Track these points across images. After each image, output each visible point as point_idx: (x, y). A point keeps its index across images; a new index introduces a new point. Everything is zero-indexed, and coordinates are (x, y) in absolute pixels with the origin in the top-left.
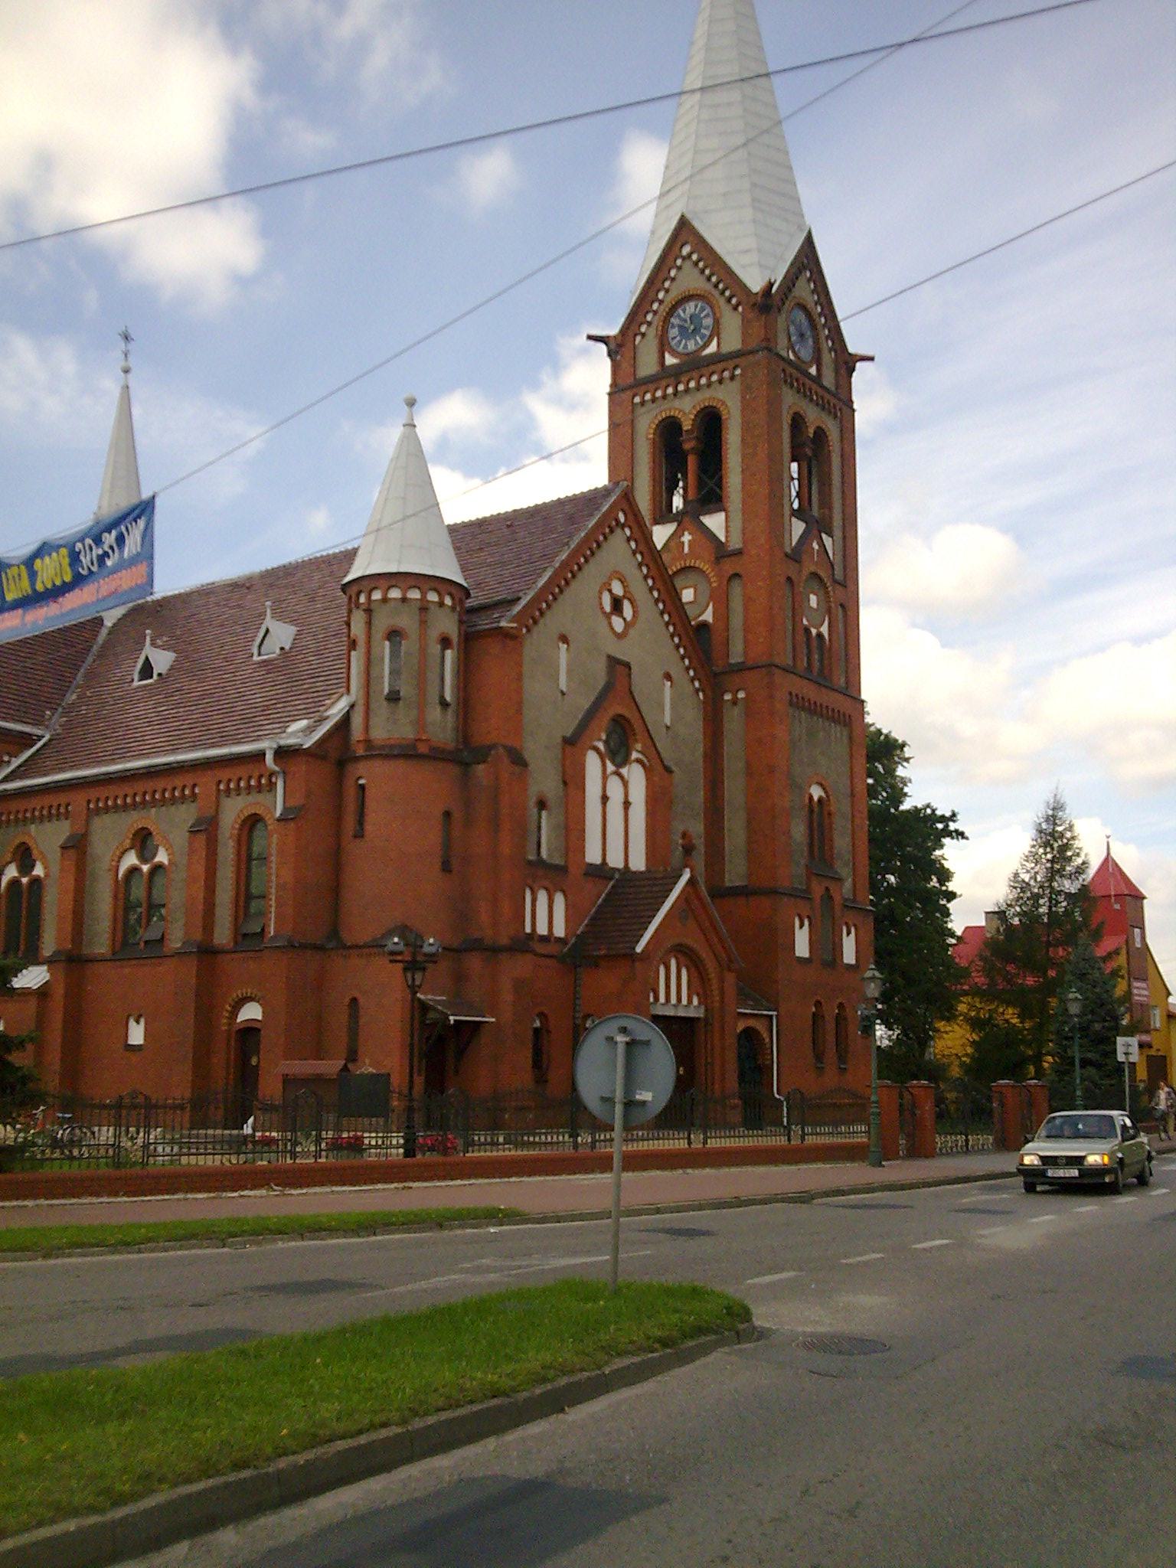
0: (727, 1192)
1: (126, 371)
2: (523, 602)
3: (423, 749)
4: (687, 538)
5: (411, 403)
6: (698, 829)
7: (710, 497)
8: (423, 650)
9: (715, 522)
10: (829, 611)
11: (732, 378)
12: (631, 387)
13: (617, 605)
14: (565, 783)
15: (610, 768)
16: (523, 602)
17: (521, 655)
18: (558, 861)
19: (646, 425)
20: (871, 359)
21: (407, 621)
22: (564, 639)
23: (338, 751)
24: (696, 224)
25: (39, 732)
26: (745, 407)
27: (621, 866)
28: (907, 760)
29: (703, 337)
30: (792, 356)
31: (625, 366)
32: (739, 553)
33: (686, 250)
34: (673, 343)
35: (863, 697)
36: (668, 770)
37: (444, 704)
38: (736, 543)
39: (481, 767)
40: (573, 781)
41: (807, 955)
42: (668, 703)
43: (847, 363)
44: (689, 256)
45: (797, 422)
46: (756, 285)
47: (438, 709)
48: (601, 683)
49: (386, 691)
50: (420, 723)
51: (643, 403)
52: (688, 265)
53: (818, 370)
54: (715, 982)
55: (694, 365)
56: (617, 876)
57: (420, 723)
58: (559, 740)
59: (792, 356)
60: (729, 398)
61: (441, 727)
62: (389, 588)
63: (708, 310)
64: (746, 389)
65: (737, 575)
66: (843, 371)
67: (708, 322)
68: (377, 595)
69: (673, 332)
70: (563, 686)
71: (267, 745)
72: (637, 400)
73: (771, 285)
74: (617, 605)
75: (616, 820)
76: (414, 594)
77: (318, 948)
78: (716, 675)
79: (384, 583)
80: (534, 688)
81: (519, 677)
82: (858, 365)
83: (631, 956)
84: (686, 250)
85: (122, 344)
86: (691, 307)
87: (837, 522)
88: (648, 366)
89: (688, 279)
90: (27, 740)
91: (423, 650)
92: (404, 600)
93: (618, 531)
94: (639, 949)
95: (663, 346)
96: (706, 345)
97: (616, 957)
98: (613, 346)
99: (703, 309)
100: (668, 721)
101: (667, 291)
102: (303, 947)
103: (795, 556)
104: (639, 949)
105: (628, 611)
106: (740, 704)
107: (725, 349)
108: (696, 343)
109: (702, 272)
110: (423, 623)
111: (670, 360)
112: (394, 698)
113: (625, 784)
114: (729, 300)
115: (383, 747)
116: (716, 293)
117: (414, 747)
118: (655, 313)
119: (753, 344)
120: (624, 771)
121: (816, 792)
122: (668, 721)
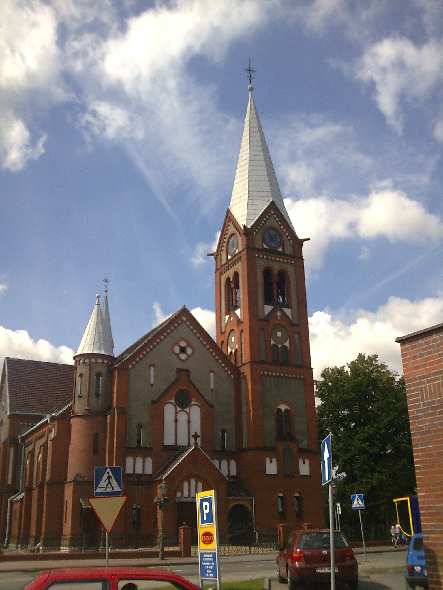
1: (106, 291)
6: (231, 427)
10: (289, 337)
14: (152, 417)
15: (178, 409)
18: (148, 445)
20: (309, 239)
22: (154, 366)
26: (242, 268)
35: (312, 367)
36: (212, 406)
37: (97, 395)
38: (242, 320)
41: (275, 472)
45: (267, 273)
48: (173, 379)
53: (227, 257)
56: (180, 449)
64: (243, 263)
74: (183, 350)
76: (93, 360)
86: (232, 238)
87: (294, 301)
92: (96, 362)
100: (212, 387)
103: (267, 319)
105: (189, 351)
111: (229, 257)
113: (189, 414)
120: (187, 410)
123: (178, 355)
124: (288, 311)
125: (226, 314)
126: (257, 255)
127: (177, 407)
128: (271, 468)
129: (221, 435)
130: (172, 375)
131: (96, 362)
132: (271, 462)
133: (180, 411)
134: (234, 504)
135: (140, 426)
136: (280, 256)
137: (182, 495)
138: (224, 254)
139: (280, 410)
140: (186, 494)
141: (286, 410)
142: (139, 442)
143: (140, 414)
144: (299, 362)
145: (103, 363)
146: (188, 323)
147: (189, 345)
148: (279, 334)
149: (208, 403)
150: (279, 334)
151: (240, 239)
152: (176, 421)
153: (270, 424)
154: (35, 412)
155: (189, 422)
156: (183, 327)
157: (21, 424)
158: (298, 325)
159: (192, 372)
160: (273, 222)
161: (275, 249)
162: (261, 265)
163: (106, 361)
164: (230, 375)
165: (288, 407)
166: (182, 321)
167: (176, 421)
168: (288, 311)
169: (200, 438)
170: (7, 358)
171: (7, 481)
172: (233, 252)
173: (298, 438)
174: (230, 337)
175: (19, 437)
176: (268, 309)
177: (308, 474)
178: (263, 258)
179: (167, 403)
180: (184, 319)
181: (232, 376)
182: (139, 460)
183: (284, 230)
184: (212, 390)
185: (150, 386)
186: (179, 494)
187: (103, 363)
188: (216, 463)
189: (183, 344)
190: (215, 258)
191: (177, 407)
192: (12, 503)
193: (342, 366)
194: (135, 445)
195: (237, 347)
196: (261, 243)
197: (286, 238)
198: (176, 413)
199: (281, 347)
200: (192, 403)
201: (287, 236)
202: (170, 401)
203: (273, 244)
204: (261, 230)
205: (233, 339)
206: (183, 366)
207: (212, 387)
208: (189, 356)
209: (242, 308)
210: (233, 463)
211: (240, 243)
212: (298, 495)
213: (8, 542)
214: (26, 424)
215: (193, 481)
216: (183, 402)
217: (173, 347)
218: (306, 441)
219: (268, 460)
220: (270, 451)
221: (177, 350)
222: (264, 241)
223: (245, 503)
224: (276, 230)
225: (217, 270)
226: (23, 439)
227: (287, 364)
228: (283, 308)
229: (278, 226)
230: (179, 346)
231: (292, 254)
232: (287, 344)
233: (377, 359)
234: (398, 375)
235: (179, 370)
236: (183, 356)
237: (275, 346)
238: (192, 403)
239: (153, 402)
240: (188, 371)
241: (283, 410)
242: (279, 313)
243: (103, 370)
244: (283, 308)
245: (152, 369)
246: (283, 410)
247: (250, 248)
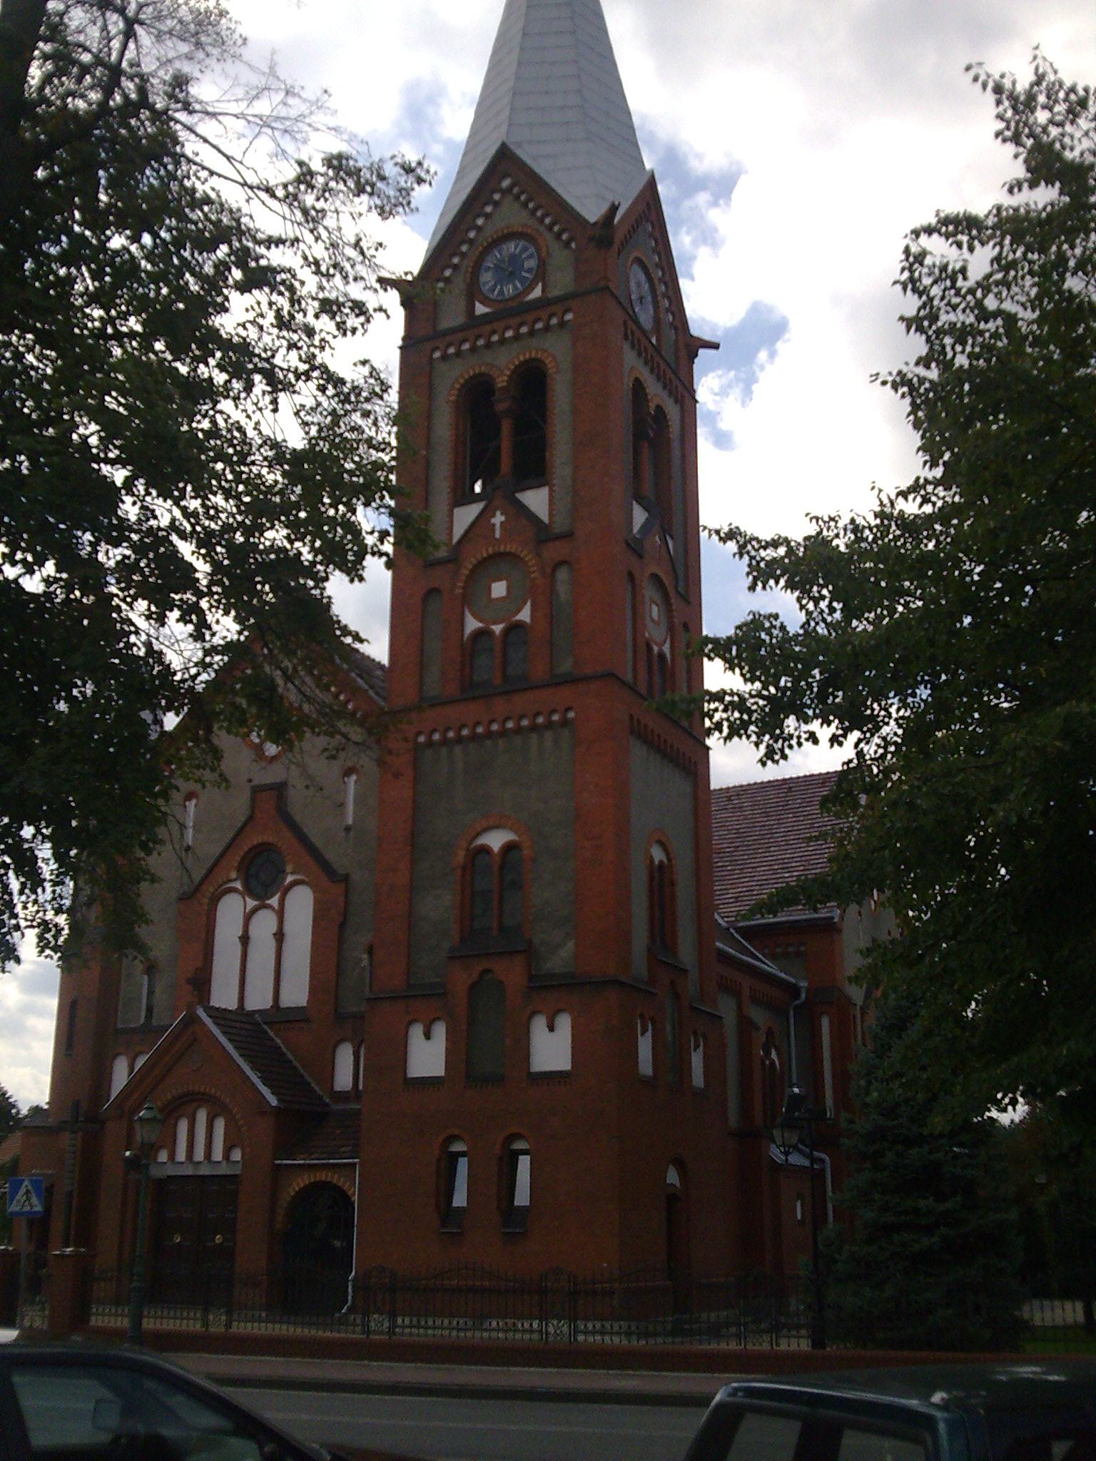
4: (498, 519)
7: (533, 468)
9: (536, 500)
12: (429, 339)
15: (251, 903)
19: (451, 378)
20: (715, 346)
24: (520, 153)
29: (523, 280)
32: (568, 536)
33: (506, 183)
34: (485, 289)
38: (560, 526)
44: (509, 190)
46: (592, 212)
52: (509, 199)
60: (556, 351)
63: (532, 250)
65: (563, 563)
67: (532, 263)
72: (437, 355)
73: (614, 208)
82: (701, 351)
84: (506, 183)
86: (511, 247)
88: (452, 317)
89: (510, 215)
95: (473, 292)
96: (531, 288)
99: (525, 249)
107: (555, 292)
108: (515, 287)
109: (525, 205)
114: (558, 236)
116: (542, 229)
121: (495, 840)
129: (365, 963)
132: (428, 1036)
134: (300, 1182)
136: (514, 321)
137: (172, 1156)
140: (181, 1156)
141: (509, 848)
152: (245, 940)
153: (440, 906)
167: (245, 940)
169: (850, 971)
177: (568, 1067)
207: (350, 822)
215: (202, 1116)
219: (417, 1031)
223: (336, 1179)
228: (519, 496)
235: (257, 790)
238: (290, 879)
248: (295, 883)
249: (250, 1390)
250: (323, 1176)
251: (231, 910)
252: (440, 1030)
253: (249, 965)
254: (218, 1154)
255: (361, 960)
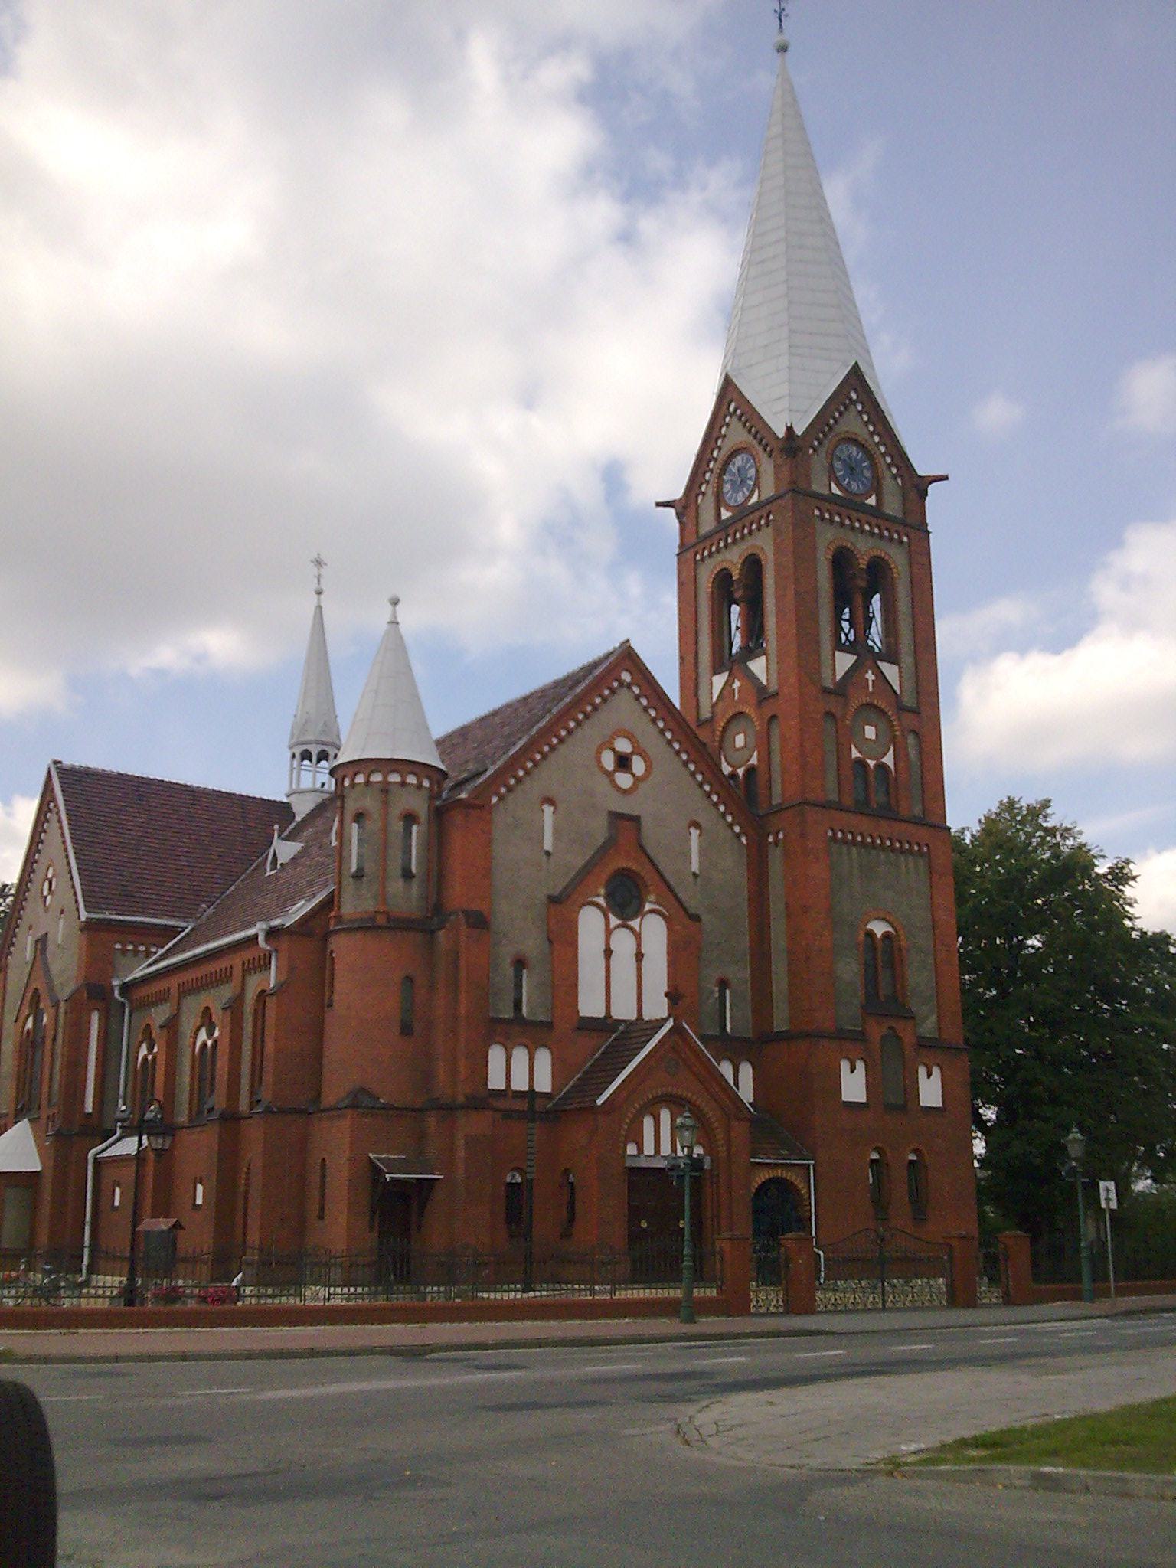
0: (178, 1348)
1: (319, 593)
2: (488, 773)
3: (381, 920)
5: (395, 602)
6: (740, 974)
8: (385, 830)
10: (893, 740)
11: (767, 524)
13: (623, 762)
14: (550, 941)
15: (614, 921)
16: (488, 773)
17: (489, 822)
20: (946, 478)
21: (370, 803)
22: (550, 801)
23: (317, 928)
25: (183, 924)
26: (777, 547)
27: (633, 1017)
28: (1134, 878)
30: (835, 490)
31: (690, 527)
36: (696, 918)
37: (407, 875)
39: (441, 933)
40: (562, 939)
41: (862, 1098)
42: (695, 846)
43: (917, 487)
45: (841, 560)
47: (401, 883)
49: (354, 868)
50: (383, 897)
51: (703, 559)
53: (719, 514)
54: (720, 1135)
55: (743, 513)
56: (621, 1028)
57: (383, 897)
58: (544, 900)
59: (835, 490)
60: (764, 543)
61: (406, 898)
62: (372, 772)
64: (778, 533)
66: (913, 495)
68: (360, 779)
69: (727, 487)
70: (548, 845)
71: (259, 929)
74: (623, 762)
75: (623, 969)
76: (395, 778)
77: (298, 1111)
78: (761, 817)
79: (350, 771)
80: (508, 851)
81: (489, 842)
82: (931, 488)
83: (593, 1109)
85: (315, 570)
86: (739, 461)
90: (173, 931)
91: (385, 830)
92: (403, 784)
93: (624, 691)
94: (599, 1102)
96: (751, 494)
97: (585, 1109)
98: (680, 509)
100: (695, 867)
101: (720, 448)
102: (282, 1111)
103: (841, 690)
104: (599, 1102)
105: (638, 766)
106: (781, 844)
107: (764, 498)
110: (386, 804)
111: (725, 514)
112: (358, 876)
113: (638, 936)
115: (352, 921)
117: (374, 919)
118: (877, 445)
119: (782, 490)
120: (635, 923)
121: (879, 928)
122: (695, 867)
123: (610, 775)
124: (890, 671)
125: (716, 672)
126: (817, 513)
127: (611, 916)
128: (854, 1086)
130: (599, 829)
131: (403, 784)
133: (618, 926)
134: (763, 1176)
135: (520, 963)
137: (640, 1150)
138: (707, 504)
139: (870, 934)
140: (649, 1149)
141: (886, 936)
142: (518, 1005)
143: (519, 929)
144: (917, 810)
145: (420, 786)
146: (636, 690)
147: (639, 751)
148: (870, 732)
149: (685, 910)
150: (870, 732)
151: (767, 467)
152: (608, 953)
153: (849, 969)
154: (154, 916)
155: (639, 956)
156: (624, 699)
157: (118, 946)
158: (916, 712)
159: (647, 824)
160: (854, 423)
161: (858, 499)
162: (827, 539)
163: (426, 783)
164: (738, 836)
165: (891, 929)
166: (621, 683)
167: (608, 953)
168: (890, 671)
170: (56, 762)
171: (83, 1102)
172: (740, 499)
173: (914, 1009)
174: (728, 734)
175: (116, 982)
176: (844, 662)
178: (832, 521)
179: (584, 905)
180: (626, 677)
181: (744, 840)
182: (520, 1055)
183: (883, 449)
184: (694, 874)
185: (544, 858)
186: (631, 1149)
187: (420, 786)
188: (726, 1069)
189: (623, 746)
190: (679, 516)
191: (611, 916)
192: (98, 1162)
193: (959, 827)
194: (508, 1014)
195: (754, 761)
196: (825, 479)
197: (887, 474)
198: (608, 932)
199: (876, 766)
200: (648, 907)
201: (889, 466)
202: (596, 899)
203: (854, 486)
204: (826, 442)
205: (740, 740)
206: (625, 807)
208: (637, 780)
209: (773, 658)
210: (496, 1082)
211: (765, 480)
212: (915, 1158)
213: (91, 1270)
214: (130, 947)
215: (665, 1115)
216: (625, 900)
217: (599, 753)
218: (933, 1018)
220: (852, 1041)
221: (608, 761)
222: (832, 475)
223: (789, 1175)
224: (862, 446)
225: (684, 548)
226: (126, 988)
227: (888, 813)
228: (880, 663)
229: (867, 437)
230: (613, 750)
231: (900, 515)
232: (889, 760)
233: (1049, 811)
234: (1104, 857)
235: (616, 817)
236: (624, 780)
237: (861, 763)
239: (553, 900)
240: (636, 820)
241: (879, 936)
242: (870, 676)
243: (419, 805)
244: (880, 663)
245: (548, 810)
246: (879, 936)
247: (797, 490)
248: (597, 905)
249: (578, 1322)
250: (779, 1173)
251: (591, 923)
252: (860, 1066)
253: (603, 973)
254: (666, 1149)
255: (713, 992)
